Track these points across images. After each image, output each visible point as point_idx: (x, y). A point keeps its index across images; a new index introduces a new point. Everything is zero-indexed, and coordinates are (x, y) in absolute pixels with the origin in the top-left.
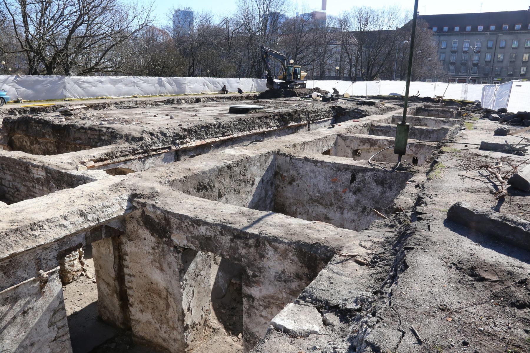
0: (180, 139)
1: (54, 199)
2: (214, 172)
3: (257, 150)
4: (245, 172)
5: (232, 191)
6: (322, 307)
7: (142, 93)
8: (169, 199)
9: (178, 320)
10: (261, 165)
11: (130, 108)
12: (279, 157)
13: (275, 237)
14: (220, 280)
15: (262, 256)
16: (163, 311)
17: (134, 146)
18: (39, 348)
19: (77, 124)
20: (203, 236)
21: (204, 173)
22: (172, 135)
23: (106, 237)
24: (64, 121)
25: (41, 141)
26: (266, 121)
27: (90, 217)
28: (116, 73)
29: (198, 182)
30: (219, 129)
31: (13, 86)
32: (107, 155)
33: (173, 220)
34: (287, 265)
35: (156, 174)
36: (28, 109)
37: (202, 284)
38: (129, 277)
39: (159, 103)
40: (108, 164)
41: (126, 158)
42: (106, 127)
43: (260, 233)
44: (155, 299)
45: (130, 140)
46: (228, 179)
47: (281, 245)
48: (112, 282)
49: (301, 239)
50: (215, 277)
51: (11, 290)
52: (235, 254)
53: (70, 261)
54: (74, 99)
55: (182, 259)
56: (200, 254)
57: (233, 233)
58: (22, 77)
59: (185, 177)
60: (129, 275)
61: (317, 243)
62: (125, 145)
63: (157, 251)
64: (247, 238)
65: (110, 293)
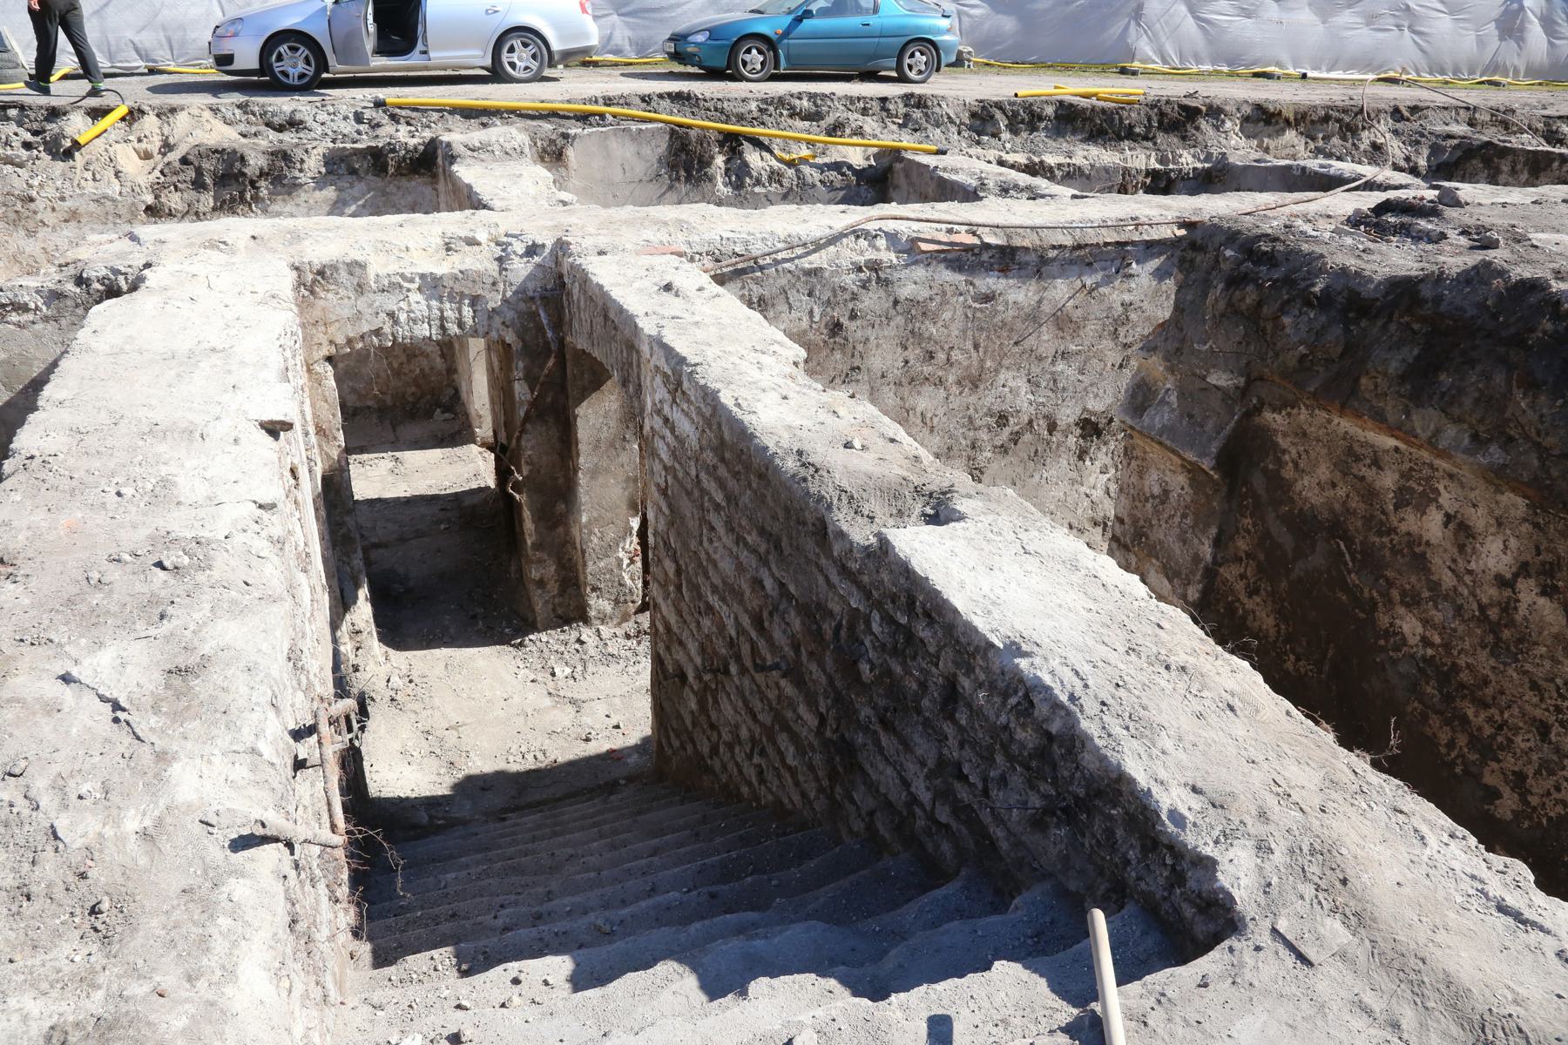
36: (1050, 110)
54: (1159, 67)
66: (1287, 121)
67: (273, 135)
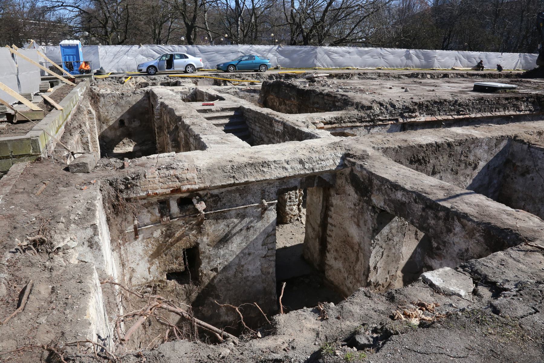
0: (409, 112)
1: (283, 147)
2: (431, 147)
3: (489, 132)
4: (468, 153)
5: (449, 170)
6: (479, 279)
7: (387, 65)
8: (377, 162)
9: (364, 274)
10: (489, 149)
11: (372, 79)
12: (515, 143)
13: (466, 214)
14: (417, 256)
15: (449, 231)
16: (352, 263)
17: (362, 114)
18: (253, 259)
19: (317, 90)
20: (399, 200)
21: (421, 146)
22: (401, 107)
23: (317, 186)
24: (307, 87)
25: (287, 102)
26: (515, 103)
27: (307, 166)
28: (366, 44)
29: (412, 154)
30: (454, 107)
31: (275, 55)
32: (336, 119)
33: (375, 182)
34: (472, 244)
35: (372, 140)
36: (284, 75)
37: (393, 249)
38: (331, 226)
39: (402, 77)
40: (336, 127)
41: (353, 124)
42: (340, 95)
43: (452, 208)
44: (348, 251)
45: (359, 108)
46: (446, 158)
47: (470, 223)
48: (317, 228)
49: (493, 222)
50: (412, 251)
51: (242, 208)
52: (424, 224)
53: (290, 205)
54: (322, 68)
55: (377, 219)
56: (396, 220)
57: (426, 203)
58: (283, 47)
59: (399, 147)
60: (331, 224)
61: (509, 229)
62: (354, 112)
63: (357, 207)
64: (438, 210)
65: (314, 236)
66: (333, 76)
67: (151, 81)
